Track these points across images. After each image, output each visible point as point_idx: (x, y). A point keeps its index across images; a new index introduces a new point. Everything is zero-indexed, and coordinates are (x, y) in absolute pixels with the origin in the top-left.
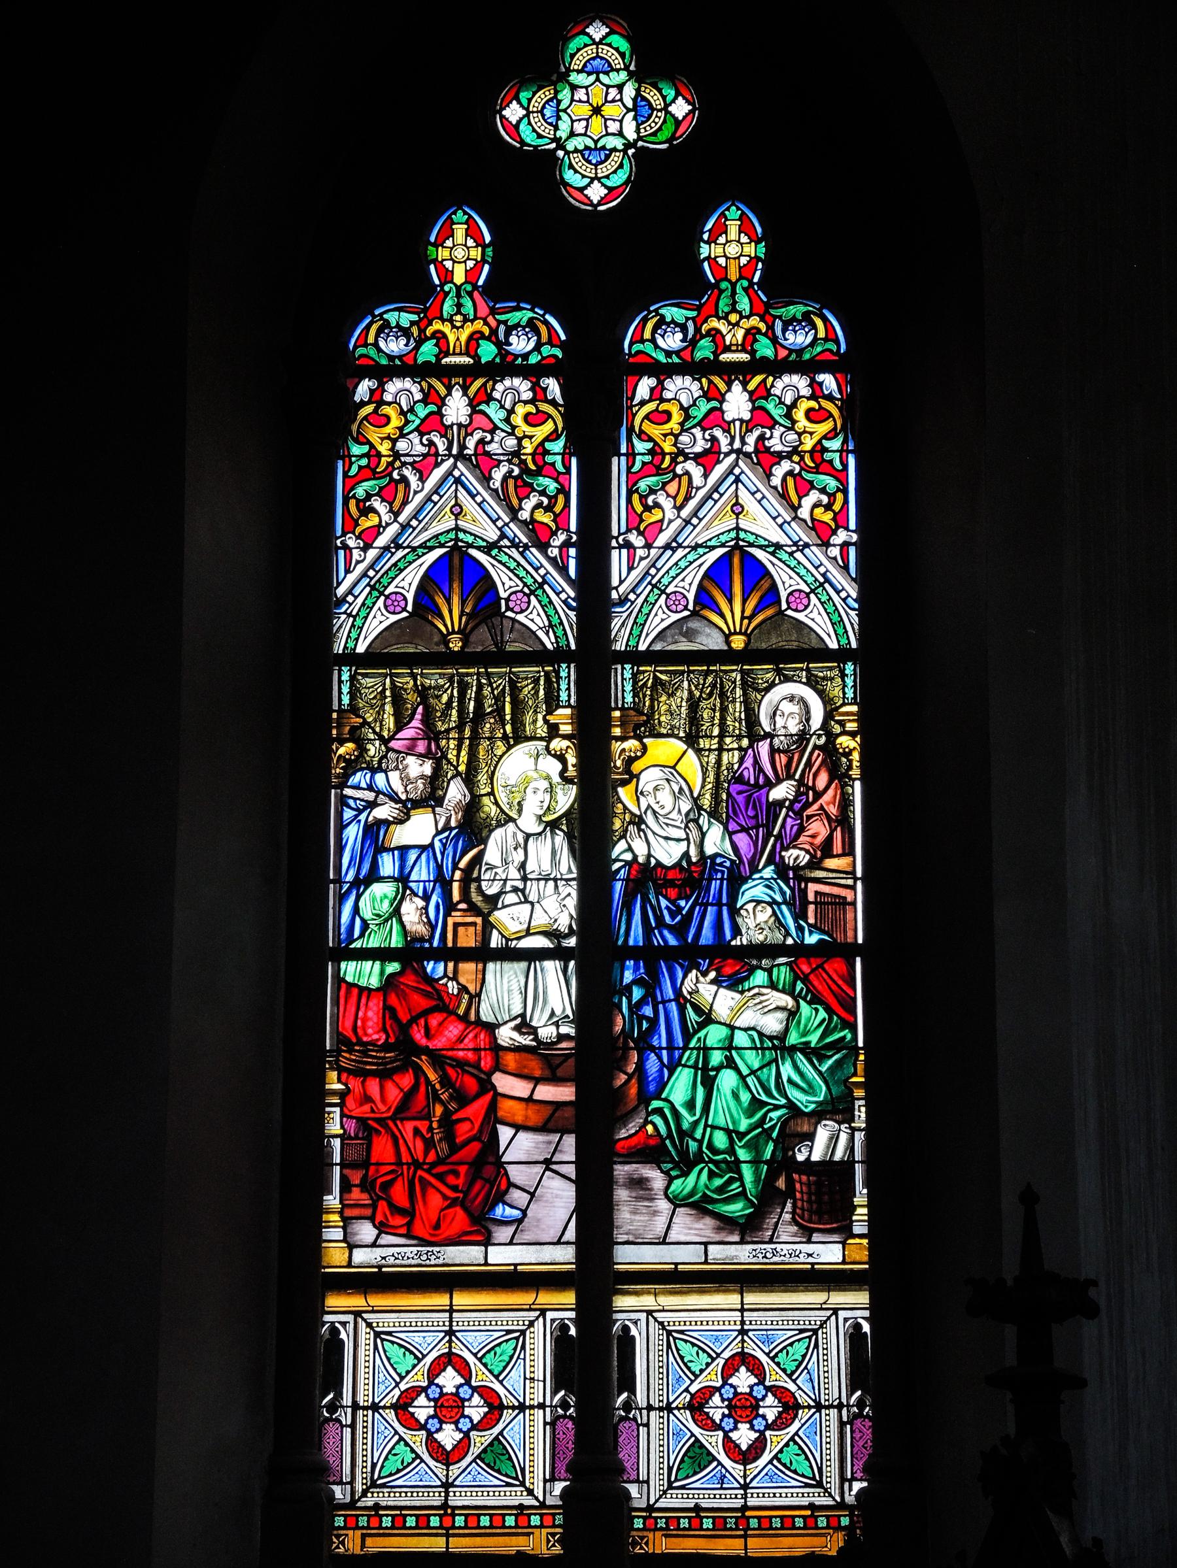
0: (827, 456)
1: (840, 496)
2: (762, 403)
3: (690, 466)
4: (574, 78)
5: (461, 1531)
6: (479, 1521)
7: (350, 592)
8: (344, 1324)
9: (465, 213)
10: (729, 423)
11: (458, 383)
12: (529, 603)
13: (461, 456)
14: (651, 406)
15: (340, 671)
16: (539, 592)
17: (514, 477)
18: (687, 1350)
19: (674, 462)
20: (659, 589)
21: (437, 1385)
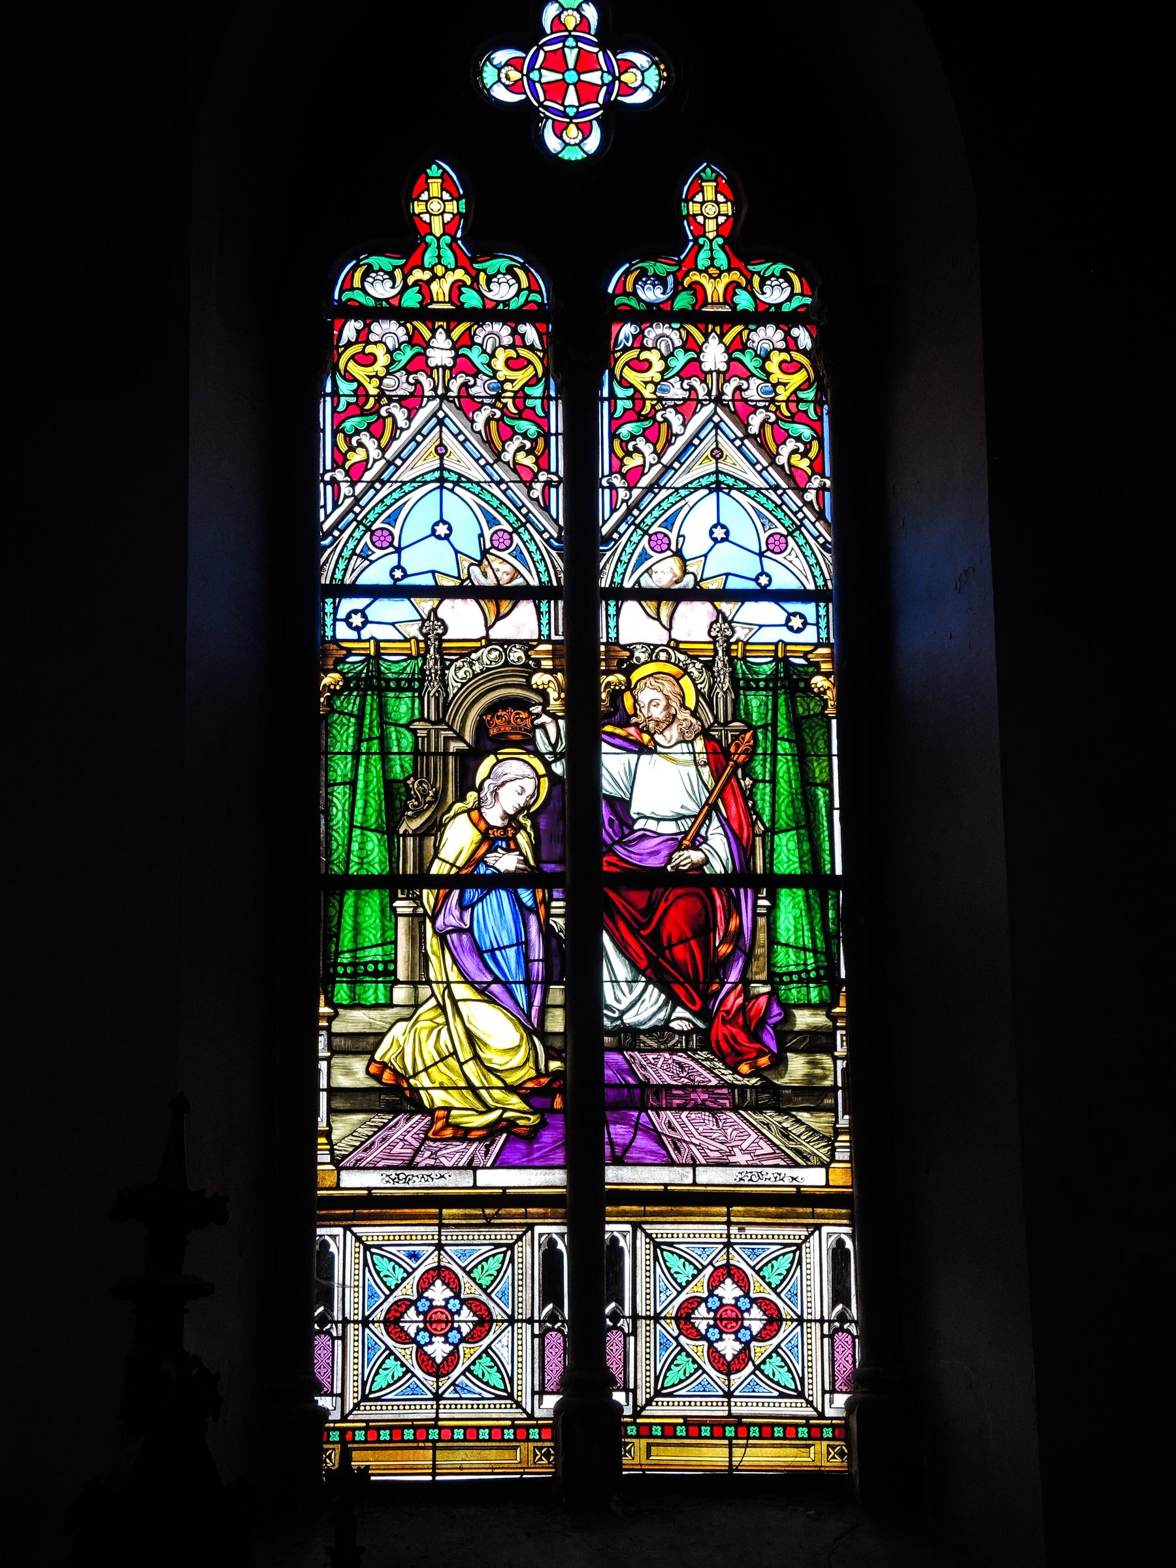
0: (529, 403)
1: (815, 444)
2: (737, 355)
7: (335, 526)
8: (334, 1237)
9: (440, 167)
10: (706, 373)
11: (441, 326)
14: (358, 348)
15: (607, 605)
16: (521, 530)
17: (496, 420)
18: (675, 1263)
20: (365, 525)
21: (427, 1299)
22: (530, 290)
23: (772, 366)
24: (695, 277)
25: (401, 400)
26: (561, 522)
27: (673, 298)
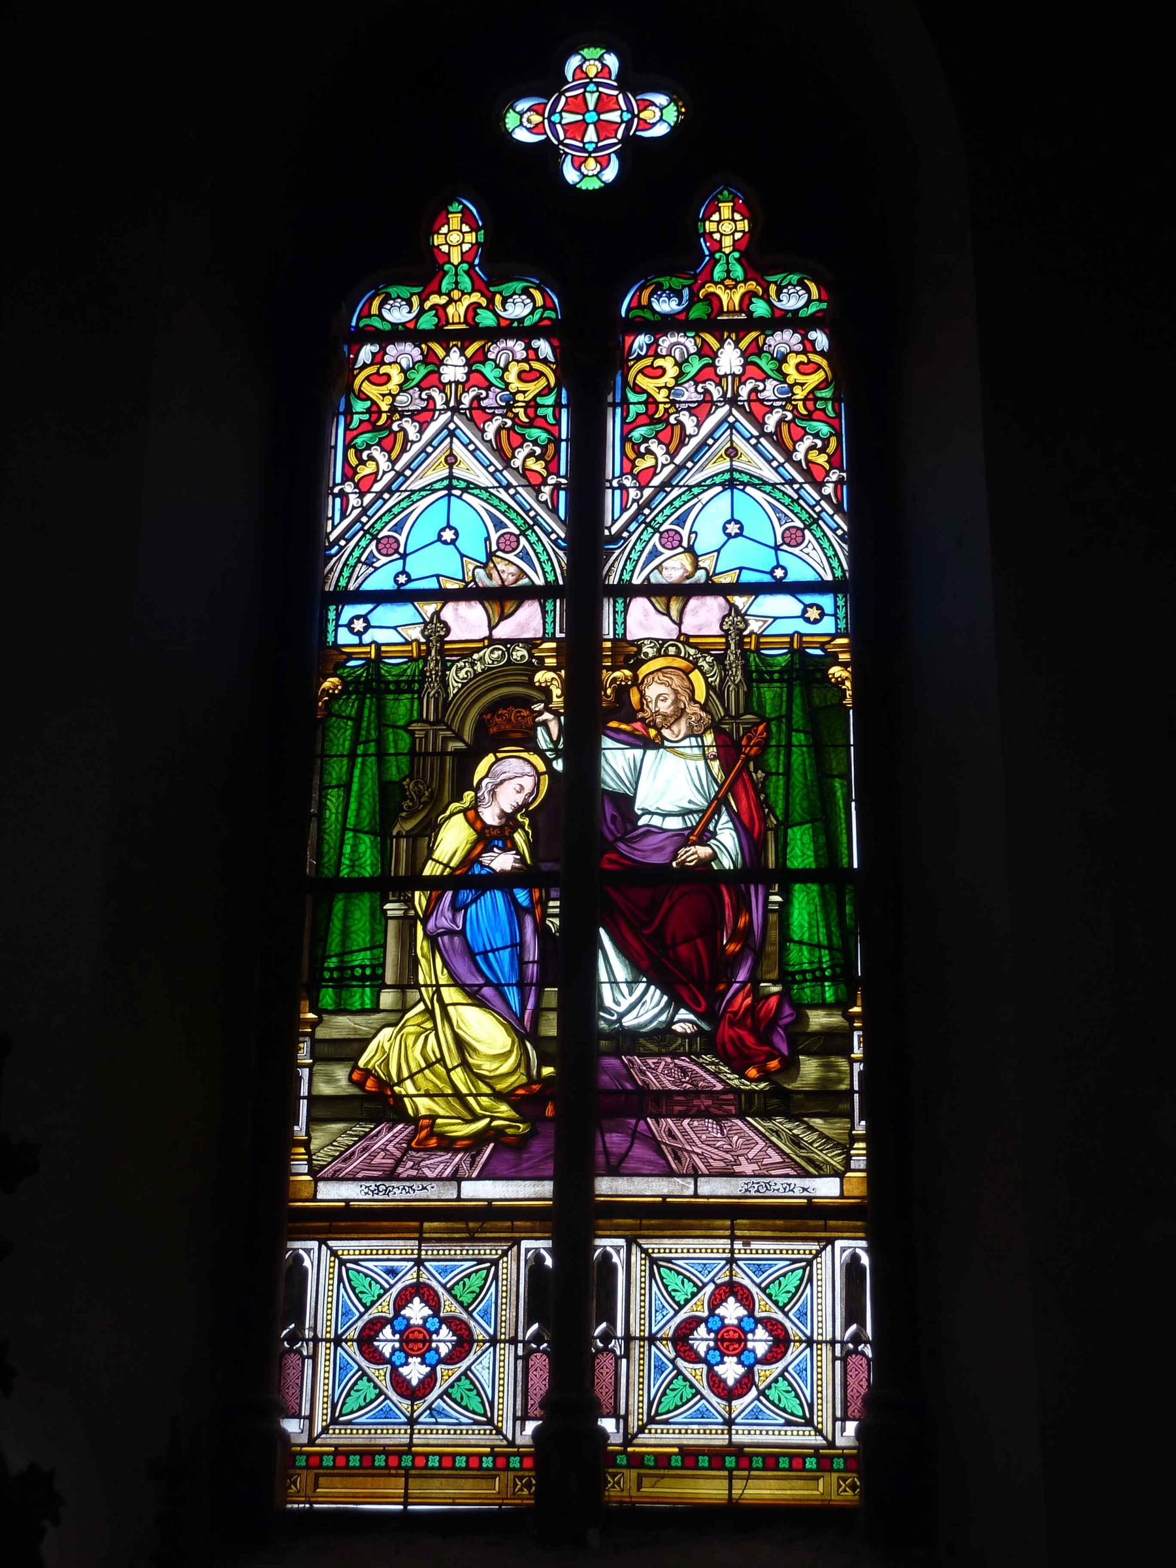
0: (541, 412)
2: (754, 359)
3: (685, 417)
5: (462, 1472)
6: (454, 1461)
8: (308, 1251)
10: (721, 377)
12: (803, 536)
13: (455, 410)
19: (390, 420)
22: (545, 307)
23: (789, 368)
24: (710, 288)
25: (413, 415)
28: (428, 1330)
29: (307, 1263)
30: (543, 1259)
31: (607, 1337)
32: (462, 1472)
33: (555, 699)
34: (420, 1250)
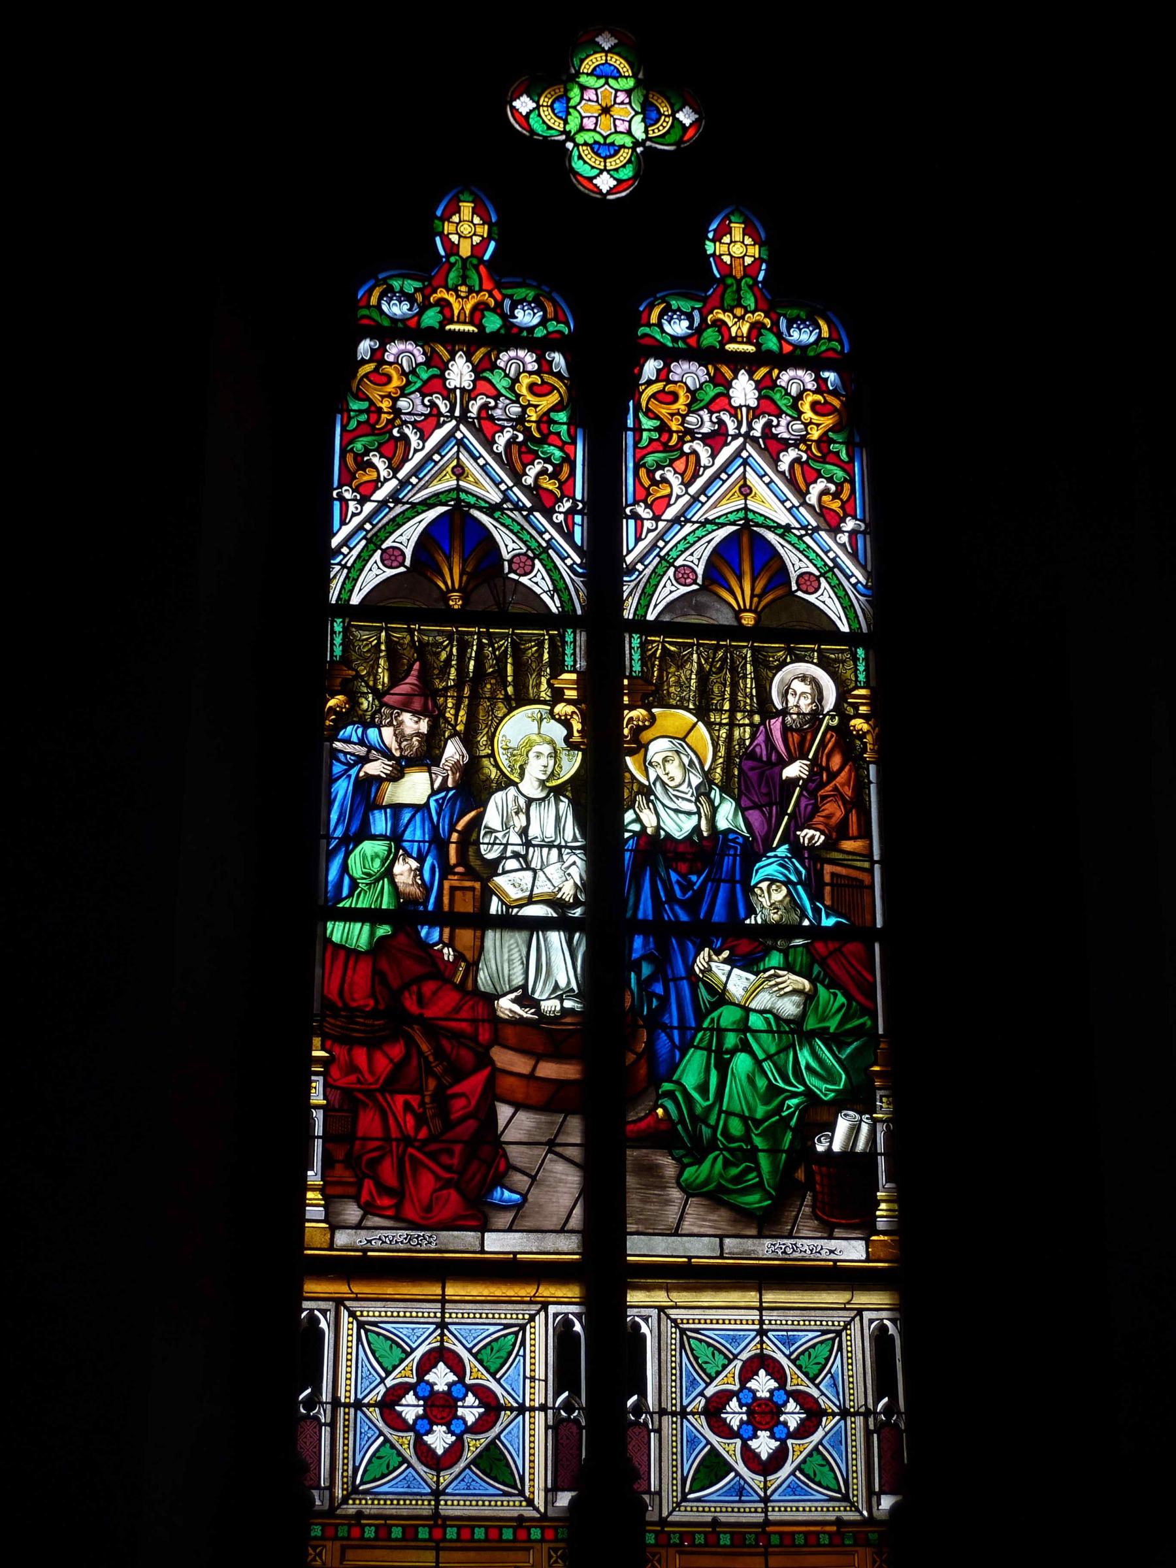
0: (554, 428)
1: (847, 486)
3: (698, 446)
4: (583, 79)
10: (736, 408)
12: (533, 566)
14: (658, 386)
15: (631, 637)
19: (682, 441)
22: (830, 339)
23: (805, 407)
24: (442, 294)
25: (706, 439)
26: (869, 569)
27: (420, 314)
28: (776, 1404)
29: (323, 1325)
30: (885, 1328)
31: (312, 1402)
32: (483, 1544)
33: (576, 734)
34: (443, 1313)
